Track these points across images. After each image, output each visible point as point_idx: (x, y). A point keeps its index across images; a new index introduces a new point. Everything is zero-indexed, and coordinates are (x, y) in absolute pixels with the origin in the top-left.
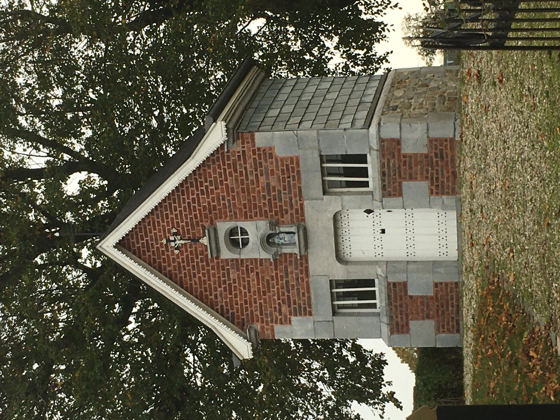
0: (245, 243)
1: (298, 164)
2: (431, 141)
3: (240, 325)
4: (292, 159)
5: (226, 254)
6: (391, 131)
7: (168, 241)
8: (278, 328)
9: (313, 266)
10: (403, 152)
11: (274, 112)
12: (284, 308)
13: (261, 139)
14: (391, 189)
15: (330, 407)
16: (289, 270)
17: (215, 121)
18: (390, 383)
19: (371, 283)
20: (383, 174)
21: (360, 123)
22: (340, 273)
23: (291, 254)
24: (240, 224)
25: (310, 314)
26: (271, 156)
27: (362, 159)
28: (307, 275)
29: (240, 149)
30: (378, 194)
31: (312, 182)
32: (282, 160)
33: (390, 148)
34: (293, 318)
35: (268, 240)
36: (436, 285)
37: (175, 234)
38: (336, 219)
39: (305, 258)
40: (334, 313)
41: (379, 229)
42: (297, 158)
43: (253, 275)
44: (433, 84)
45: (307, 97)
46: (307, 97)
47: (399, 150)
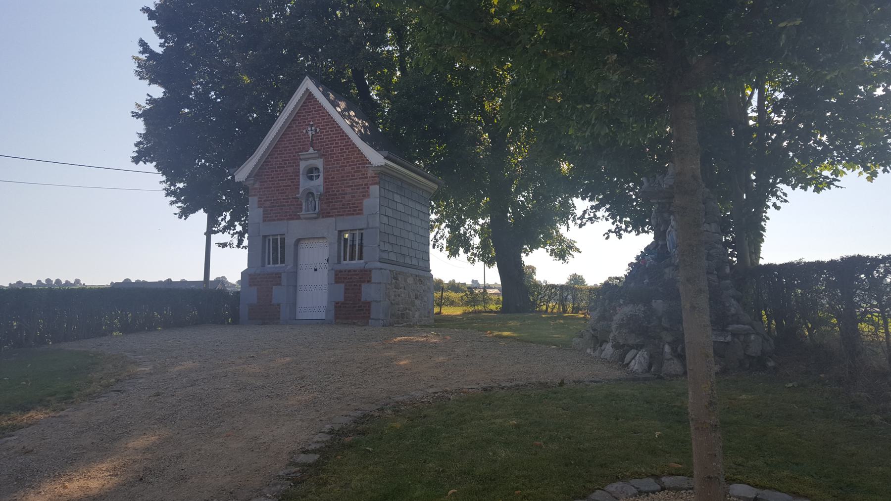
0: (311, 178)
1: (358, 214)
2: (369, 303)
3: (256, 174)
4: (362, 210)
5: (303, 165)
6: (375, 276)
7: (312, 126)
8: (256, 199)
9: (295, 223)
10: (363, 285)
11: (397, 198)
12: (268, 203)
13: (374, 189)
14: (339, 276)
15: (608, 206)
17: (385, 158)
18: (884, 171)
19: (283, 262)
20: (349, 271)
21: (385, 255)
22: (290, 242)
23: (301, 208)
24: (321, 174)
25: (264, 221)
26: (364, 196)
27: (361, 258)
28: (288, 219)
29: (369, 175)
30: (338, 267)
31: (345, 223)
32: (361, 203)
33: (365, 275)
34: (261, 210)
35: (310, 194)
36: (279, 305)
37: (316, 130)
38: (324, 238)
39: (299, 218)
40: (265, 237)
41: (318, 267)
42: (362, 214)
43: (289, 183)
44: (417, 302)
45: (411, 220)
46: (411, 220)
47: (364, 282)
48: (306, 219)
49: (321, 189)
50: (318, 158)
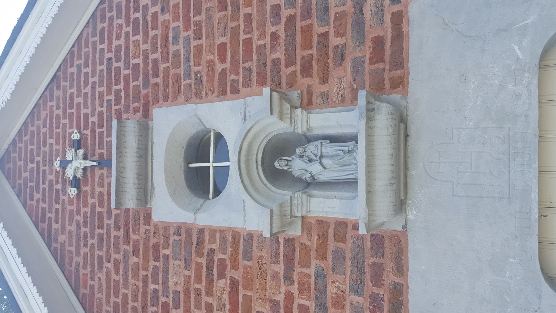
5: (168, 208)
16: (331, 290)
48: (401, 205)
49: (259, 101)
50: (145, 132)
